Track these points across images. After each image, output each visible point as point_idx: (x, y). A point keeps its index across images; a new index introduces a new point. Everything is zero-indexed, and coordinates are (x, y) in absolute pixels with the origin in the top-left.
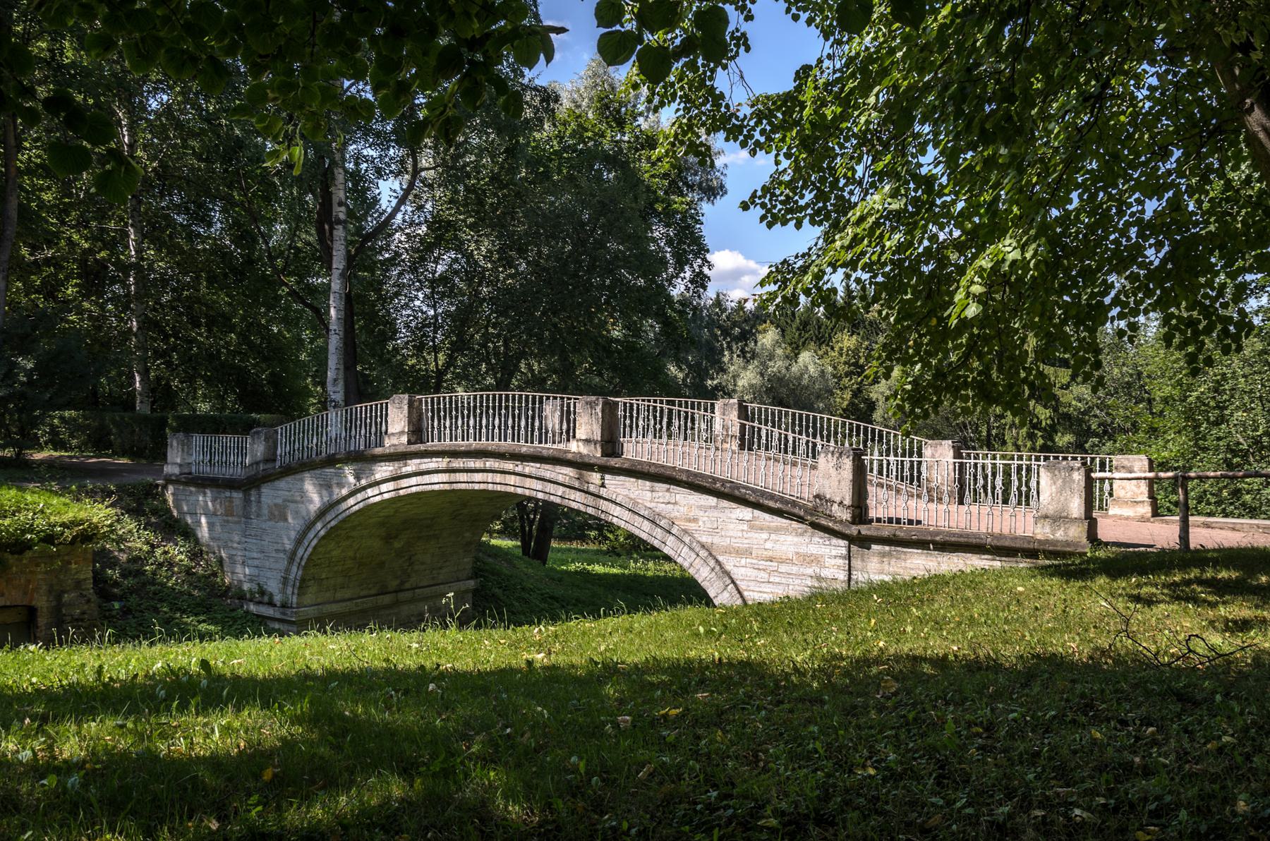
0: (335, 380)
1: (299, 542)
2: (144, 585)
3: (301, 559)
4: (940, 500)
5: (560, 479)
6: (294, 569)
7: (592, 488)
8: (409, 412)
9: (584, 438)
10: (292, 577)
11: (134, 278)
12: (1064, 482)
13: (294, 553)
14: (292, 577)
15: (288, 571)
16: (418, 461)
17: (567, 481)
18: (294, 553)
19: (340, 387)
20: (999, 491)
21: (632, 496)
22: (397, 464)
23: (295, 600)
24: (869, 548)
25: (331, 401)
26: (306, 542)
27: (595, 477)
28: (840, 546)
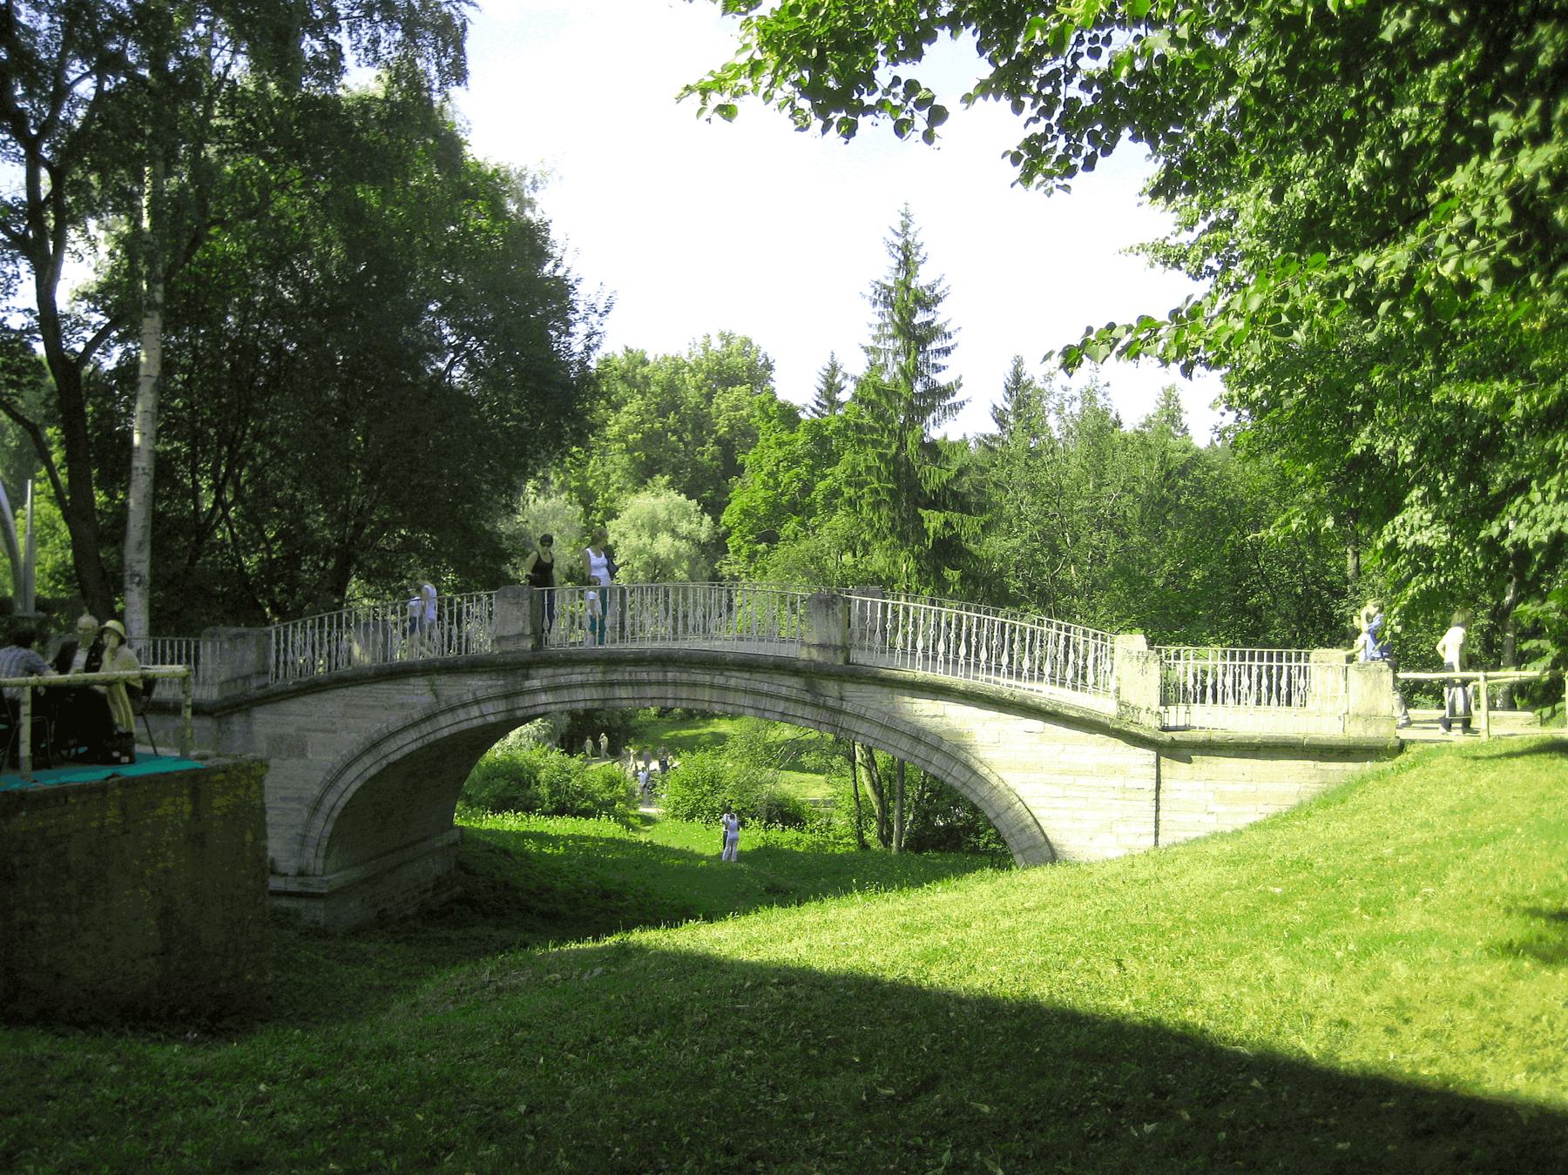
0: (140, 544)
1: (329, 786)
2: (901, 1023)
3: (332, 809)
4: (1062, 684)
5: (784, 691)
6: (319, 823)
7: (830, 702)
8: (532, 609)
9: (816, 642)
10: (314, 834)
11: (84, 415)
12: (1374, 684)
13: (319, 802)
14: (314, 834)
15: (308, 826)
16: (549, 671)
17: (794, 694)
18: (319, 802)
19: (145, 555)
20: (1284, 692)
21: (884, 709)
22: (510, 679)
23: (320, 863)
24: (1190, 761)
25: (133, 575)
26: (342, 785)
27: (831, 688)
28: (1149, 756)
